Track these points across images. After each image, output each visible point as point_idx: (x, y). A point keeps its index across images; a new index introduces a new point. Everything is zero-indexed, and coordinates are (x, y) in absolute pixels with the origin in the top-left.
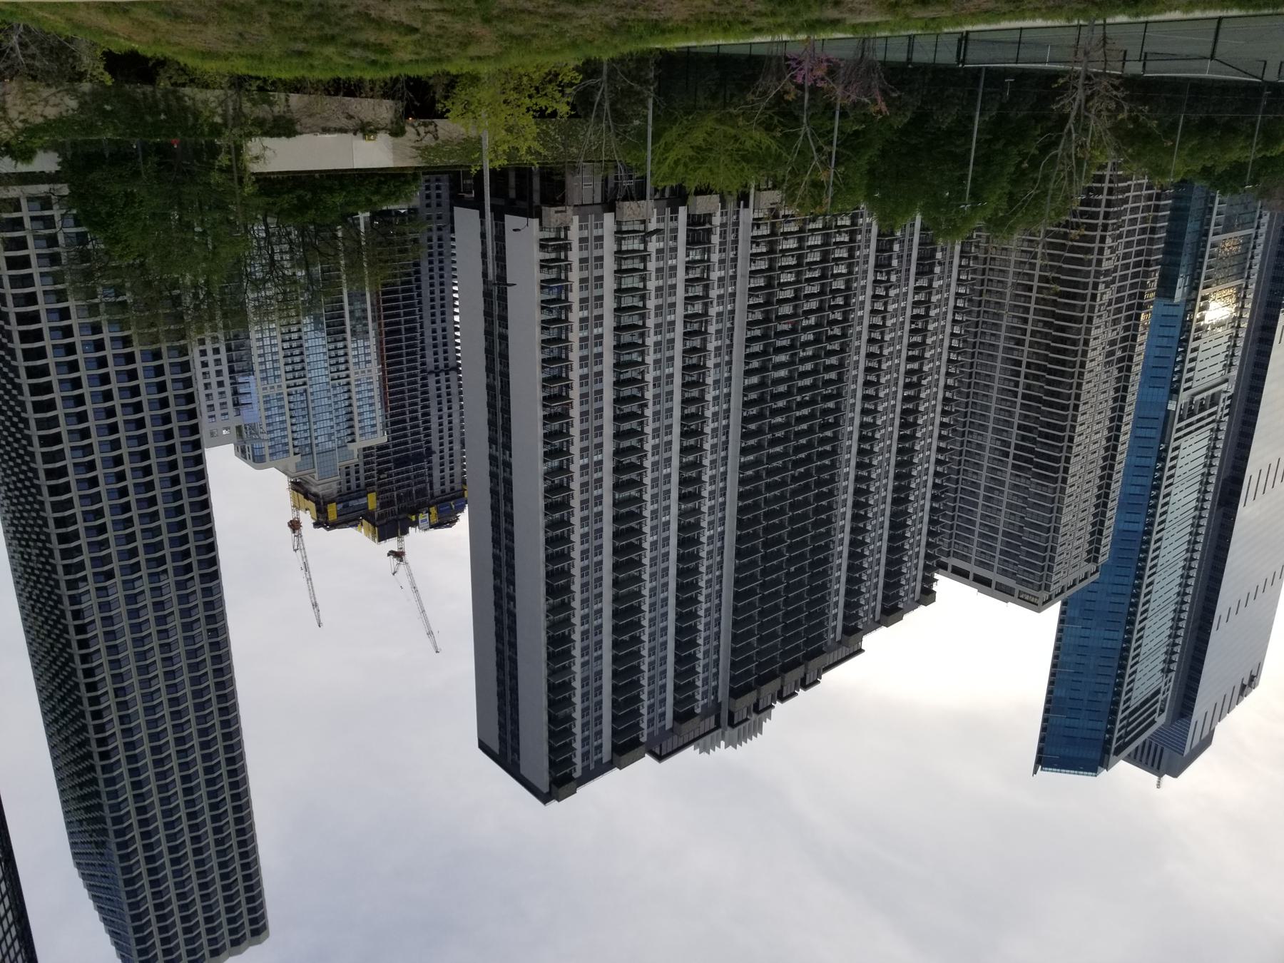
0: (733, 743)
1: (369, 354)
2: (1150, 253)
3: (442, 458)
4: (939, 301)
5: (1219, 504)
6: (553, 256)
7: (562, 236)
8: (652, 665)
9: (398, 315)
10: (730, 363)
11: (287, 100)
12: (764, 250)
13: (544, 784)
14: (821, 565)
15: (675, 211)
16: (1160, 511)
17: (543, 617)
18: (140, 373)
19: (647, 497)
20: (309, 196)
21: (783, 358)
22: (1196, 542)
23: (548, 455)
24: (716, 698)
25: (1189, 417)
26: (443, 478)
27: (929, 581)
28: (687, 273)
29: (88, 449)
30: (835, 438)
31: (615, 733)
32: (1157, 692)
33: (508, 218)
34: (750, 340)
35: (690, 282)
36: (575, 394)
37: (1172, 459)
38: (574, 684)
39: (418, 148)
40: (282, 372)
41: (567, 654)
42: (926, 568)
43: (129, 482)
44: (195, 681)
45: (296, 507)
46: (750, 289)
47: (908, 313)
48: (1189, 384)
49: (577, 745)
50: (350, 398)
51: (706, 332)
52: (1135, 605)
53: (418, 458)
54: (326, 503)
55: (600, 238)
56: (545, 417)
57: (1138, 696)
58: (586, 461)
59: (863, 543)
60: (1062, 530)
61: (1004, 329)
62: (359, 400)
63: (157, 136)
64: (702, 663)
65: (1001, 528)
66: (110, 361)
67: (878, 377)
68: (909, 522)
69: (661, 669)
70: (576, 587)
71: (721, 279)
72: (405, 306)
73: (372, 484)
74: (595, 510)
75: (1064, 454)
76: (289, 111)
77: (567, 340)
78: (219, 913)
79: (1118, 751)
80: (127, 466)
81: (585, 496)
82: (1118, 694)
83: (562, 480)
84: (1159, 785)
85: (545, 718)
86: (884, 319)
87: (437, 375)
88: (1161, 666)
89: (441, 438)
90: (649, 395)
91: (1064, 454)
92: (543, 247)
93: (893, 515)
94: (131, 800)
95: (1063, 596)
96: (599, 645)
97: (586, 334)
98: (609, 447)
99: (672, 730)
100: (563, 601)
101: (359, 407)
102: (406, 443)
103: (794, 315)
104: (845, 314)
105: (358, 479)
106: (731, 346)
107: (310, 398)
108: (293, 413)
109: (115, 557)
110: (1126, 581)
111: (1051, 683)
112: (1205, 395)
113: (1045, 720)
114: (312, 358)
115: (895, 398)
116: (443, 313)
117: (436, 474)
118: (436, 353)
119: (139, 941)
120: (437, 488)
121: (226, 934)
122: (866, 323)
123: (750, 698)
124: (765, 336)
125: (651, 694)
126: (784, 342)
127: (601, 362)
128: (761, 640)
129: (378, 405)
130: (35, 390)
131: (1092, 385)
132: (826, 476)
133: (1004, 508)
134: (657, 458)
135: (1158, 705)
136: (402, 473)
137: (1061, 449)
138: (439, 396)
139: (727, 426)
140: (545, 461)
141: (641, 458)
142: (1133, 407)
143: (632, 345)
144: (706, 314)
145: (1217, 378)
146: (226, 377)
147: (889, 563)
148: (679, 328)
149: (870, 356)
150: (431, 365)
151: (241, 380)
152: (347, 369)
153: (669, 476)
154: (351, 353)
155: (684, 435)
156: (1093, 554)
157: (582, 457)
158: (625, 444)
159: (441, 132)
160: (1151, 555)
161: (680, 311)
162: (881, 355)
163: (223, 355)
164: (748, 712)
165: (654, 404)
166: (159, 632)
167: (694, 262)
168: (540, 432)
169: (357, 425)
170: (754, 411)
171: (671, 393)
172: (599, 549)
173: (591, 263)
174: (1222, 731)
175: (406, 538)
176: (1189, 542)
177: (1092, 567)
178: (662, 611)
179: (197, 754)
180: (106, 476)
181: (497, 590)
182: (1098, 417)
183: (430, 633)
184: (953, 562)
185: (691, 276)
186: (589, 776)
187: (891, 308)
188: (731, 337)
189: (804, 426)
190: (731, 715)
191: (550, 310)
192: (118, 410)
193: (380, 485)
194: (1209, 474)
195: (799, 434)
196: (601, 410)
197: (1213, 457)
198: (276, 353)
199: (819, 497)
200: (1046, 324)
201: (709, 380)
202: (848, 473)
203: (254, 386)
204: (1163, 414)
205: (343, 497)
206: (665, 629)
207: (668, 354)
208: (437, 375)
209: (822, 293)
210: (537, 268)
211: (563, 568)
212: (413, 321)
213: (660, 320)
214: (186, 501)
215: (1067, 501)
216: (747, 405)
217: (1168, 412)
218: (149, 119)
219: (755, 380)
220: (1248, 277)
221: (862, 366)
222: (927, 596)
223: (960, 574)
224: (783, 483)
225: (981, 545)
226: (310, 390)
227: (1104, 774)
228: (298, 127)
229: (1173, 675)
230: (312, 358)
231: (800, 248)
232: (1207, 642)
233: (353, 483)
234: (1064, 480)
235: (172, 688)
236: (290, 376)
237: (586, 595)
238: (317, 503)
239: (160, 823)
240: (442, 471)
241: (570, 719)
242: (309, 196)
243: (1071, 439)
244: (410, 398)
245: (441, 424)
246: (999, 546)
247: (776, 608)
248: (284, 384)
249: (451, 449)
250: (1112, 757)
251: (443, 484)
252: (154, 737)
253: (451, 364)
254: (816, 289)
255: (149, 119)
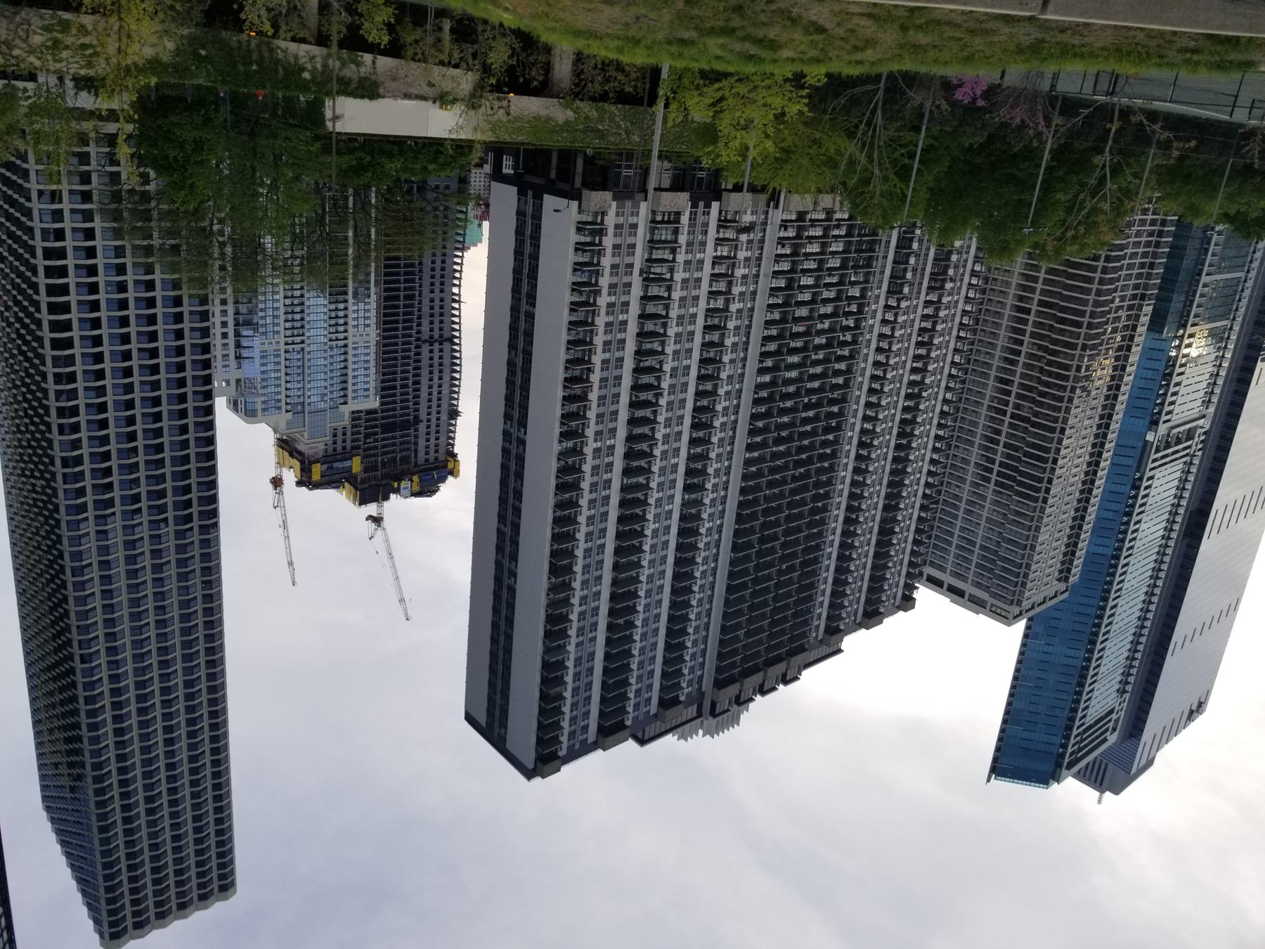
0: (711, 732)
1: (368, 318)
2: (1146, 287)
3: (428, 427)
4: (946, 316)
5: (1185, 535)
6: (588, 239)
7: (599, 220)
8: (642, 651)
9: (398, 282)
10: (744, 359)
11: (374, 62)
12: (788, 252)
13: (529, 760)
14: (811, 564)
15: (708, 206)
16: (1129, 537)
17: (544, 595)
18: (160, 319)
19: (653, 485)
20: (368, 158)
21: (795, 359)
22: (1160, 570)
23: (564, 436)
24: (700, 688)
25: (1166, 448)
26: (427, 447)
27: (910, 588)
28: (713, 268)
29: (101, 391)
30: (836, 441)
31: (602, 714)
32: (1111, 712)
33: (546, 197)
34: (767, 339)
35: (715, 277)
36: (595, 378)
37: (1146, 488)
38: (567, 663)
39: (490, 123)
40: (281, 328)
41: (563, 634)
42: (909, 575)
43: (139, 427)
44: (185, 632)
45: (280, 464)
46: (772, 289)
47: (916, 326)
48: (1169, 417)
49: (565, 724)
50: (346, 360)
51: (725, 328)
52: (1099, 626)
53: (405, 425)
54: (311, 463)
55: (634, 226)
56: (564, 398)
57: (1094, 712)
58: (599, 444)
59: (852, 547)
60: (1038, 548)
61: (999, 348)
62: (354, 363)
63: (245, 86)
64: (638, 645)
65: (979, 542)
66: (132, 304)
67: (882, 385)
68: (897, 530)
69: (651, 654)
70: (578, 568)
71: (744, 277)
72: (406, 274)
73: (358, 448)
74: (603, 493)
75: (1047, 475)
76: (375, 73)
77: (593, 324)
78: (189, 866)
79: (1070, 766)
80: (138, 411)
81: (595, 479)
82: (1075, 710)
83: (574, 462)
84: (1099, 801)
85: (537, 694)
86: (893, 329)
87: (431, 345)
88: (1117, 687)
89: (429, 407)
90: (665, 385)
91: (1047, 475)
92: (579, 230)
93: (883, 521)
94: (112, 747)
95: (1031, 614)
96: (594, 626)
97: (611, 319)
98: (622, 433)
99: (655, 715)
100: (564, 581)
101: (354, 370)
102: (395, 409)
103: (809, 318)
104: (857, 321)
105: (344, 441)
106: (747, 343)
107: (307, 357)
108: (289, 371)
109: (170, 507)
110: (1091, 602)
111: (1011, 695)
112: (1181, 429)
113: (1002, 731)
114: (312, 317)
115: (895, 408)
116: (442, 284)
117: (422, 443)
118: (432, 323)
119: (109, 890)
120: (421, 456)
121: (195, 888)
122: (876, 332)
123: (733, 690)
124: (780, 336)
125: (640, 678)
126: (798, 344)
127: (623, 349)
128: (749, 634)
129: (373, 370)
130: (55, 326)
131: (1079, 410)
132: (824, 478)
133: (983, 523)
134: (666, 447)
135: (1111, 724)
136: (388, 439)
137: (1044, 470)
138: (431, 366)
139: (736, 422)
140: (560, 442)
141: (651, 447)
142: (1115, 435)
143: (653, 334)
144: (726, 309)
145: (1195, 413)
146: (230, 330)
147: (875, 567)
148: (700, 322)
149: (877, 364)
150: (425, 336)
151: (244, 333)
152: (346, 331)
153: (676, 465)
154: (352, 315)
155: (695, 426)
156: (1064, 574)
157: (596, 441)
158: (638, 431)
159: (513, 108)
160: (1117, 579)
161: (703, 304)
162: (887, 364)
163: (230, 309)
164: (730, 703)
165: (669, 394)
166: (154, 580)
167: (722, 257)
168: (559, 412)
169: (350, 388)
170: (763, 409)
171: (686, 384)
172: (603, 532)
173: (624, 250)
174: (1162, 757)
175: (386, 504)
176: (1153, 569)
177: (1062, 586)
178: (657, 598)
179: (181, 705)
180: (117, 419)
181: (498, 565)
182: (1082, 442)
183: (402, 600)
184: (928, 570)
185: (716, 271)
186: (573, 755)
187: (901, 319)
188: (748, 334)
189: (808, 428)
190: (713, 705)
191: (581, 293)
192: (135, 354)
193: (366, 450)
194: (1179, 505)
195: (803, 435)
196: (617, 395)
197: (1184, 489)
198: (277, 309)
199: (816, 498)
200: (1040, 347)
201: (724, 375)
202: (844, 477)
203: (256, 344)
204: (1141, 444)
205: (328, 458)
206: (658, 616)
207: (687, 346)
208: (431, 345)
209: (838, 299)
210: (571, 250)
211: (567, 549)
212: (412, 289)
213: (682, 312)
214: (192, 451)
215: (1045, 520)
216: (757, 402)
217: (1146, 442)
218: (241, 68)
219: (767, 378)
220: (1234, 319)
221: (868, 374)
222: (907, 602)
223: (935, 583)
224: (783, 482)
225: (958, 556)
226: (307, 349)
227: (1055, 787)
228: (381, 91)
229: (1127, 696)
230: (312, 317)
231: (822, 253)
232: (1161, 667)
233: (339, 445)
234: (1045, 501)
235: (162, 637)
236: (289, 333)
237: (586, 576)
238: (302, 462)
239: (138, 771)
240: (428, 440)
241: (561, 698)
242: (368, 158)
243: (1055, 461)
244: (403, 365)
245: (430, 394)
246: (975, 559)
247: (765, 604)
248: (283, 340)
249: (438, 419)
250: (1064, 772)
251: (427, 453)
252: (140, 685)
253: (446, 335)
254: (832, 295)
255: (241, 68)
